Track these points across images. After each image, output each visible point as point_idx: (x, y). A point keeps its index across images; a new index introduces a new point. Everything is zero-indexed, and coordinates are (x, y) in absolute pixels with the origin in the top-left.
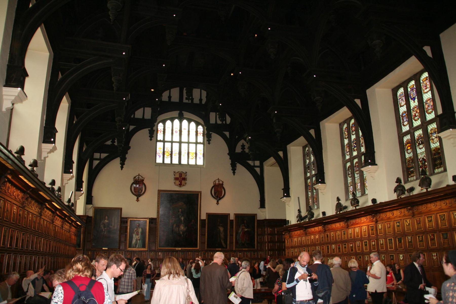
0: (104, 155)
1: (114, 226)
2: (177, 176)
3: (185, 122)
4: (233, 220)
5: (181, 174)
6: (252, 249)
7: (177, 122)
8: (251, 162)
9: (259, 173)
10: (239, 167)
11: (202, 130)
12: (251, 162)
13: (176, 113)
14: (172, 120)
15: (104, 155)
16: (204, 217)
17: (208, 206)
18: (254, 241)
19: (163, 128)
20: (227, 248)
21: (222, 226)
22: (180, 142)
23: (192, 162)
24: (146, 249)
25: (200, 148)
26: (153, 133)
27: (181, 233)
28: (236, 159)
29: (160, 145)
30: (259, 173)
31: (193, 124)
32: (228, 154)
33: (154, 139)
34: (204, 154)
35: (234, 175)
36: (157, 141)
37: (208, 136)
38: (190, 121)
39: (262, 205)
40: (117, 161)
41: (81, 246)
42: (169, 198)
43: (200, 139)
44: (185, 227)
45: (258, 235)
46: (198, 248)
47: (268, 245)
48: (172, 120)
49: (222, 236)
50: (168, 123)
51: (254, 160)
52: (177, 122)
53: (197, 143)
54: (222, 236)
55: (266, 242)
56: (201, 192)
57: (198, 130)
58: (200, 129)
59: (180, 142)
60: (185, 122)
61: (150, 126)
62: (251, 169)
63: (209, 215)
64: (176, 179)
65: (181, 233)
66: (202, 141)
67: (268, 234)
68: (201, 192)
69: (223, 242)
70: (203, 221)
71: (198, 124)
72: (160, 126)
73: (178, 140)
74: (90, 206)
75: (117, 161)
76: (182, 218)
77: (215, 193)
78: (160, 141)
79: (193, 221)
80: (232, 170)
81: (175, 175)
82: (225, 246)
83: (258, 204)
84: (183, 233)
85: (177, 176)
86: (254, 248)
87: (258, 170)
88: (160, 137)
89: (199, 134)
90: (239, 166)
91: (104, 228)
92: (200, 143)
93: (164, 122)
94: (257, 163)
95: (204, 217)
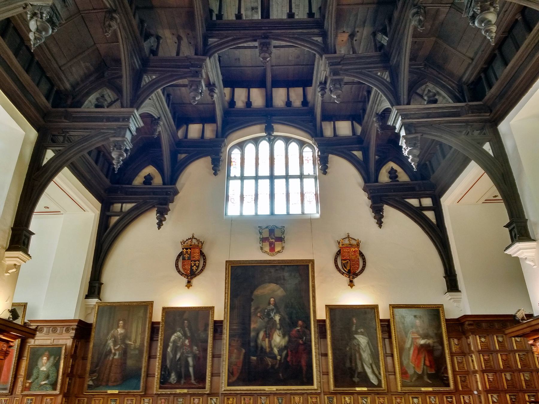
0: (127, 207)
1: (135, 342)
2: (266, 234)
3: (279, 145)
4: (324, 321)
5: (272, 231)
6: (441, 389)
7: (264, 145)
8: (414, 202)
9: (434, 220)
10: (389, 211)
11: (311, 154)
12: (414, 202)
13: (257, 131)
14: (256, 141)
15: (127, 207)
16: (321, 314)
17: (333, 293)
18: (446, 368)
19: (239, 156)
20: (380, 385)
21: (362, 334)
22: (272, 177)
23: (296, 210)
24: (57, 392)
25: (310, 185)
26: (218, 164)
27: (276, 351)
28: (381, 199)
29: (234, 186)
30: (434, 220)
31: (294, 147)
32: (364, 190)
33: (222, 174)
34: (316, 194)
35: (380, 226)
36: (229, 178)
37: (323, 163)
38: (287, 140)
39: (452, 285)
40: (152, 217)
41: (59, 386)
42: (242, 279)
43: (309, 168)
44: (284, 336)
45: (452, 354)
46: (315, 387)
47: (483, 379)
48: (256, 141)
49: (366, 355)
50: (250, 148)
51: (419, 197)
52: (264, 145)
53: (301, 177)
54: (366, 355)
55: (475, 372)
56: (312, 261)
57: (304, 154)
58: (308, 153)
59: (272, 177)
60: (279, 145)
61: (213, 152)
62: (416, 214)
63: (332, 309)
64: (263, 240)
65: (276, 351)
66: (312, 173)
67: (479, 352)
68: (312, 261)
69: (369, 371)
70: (321, 324)
71: (302, 144)
72: (236, 154)
73: (268, 174)
74: (94, 301)
75: (152, 217)
76: (277, 318)
77: (344, 266)
78: (235, 178)
79: (300, 322)
80: (375, 218)
81: (261, 233)
82: (374, 381)
83: (443, 283)
84: (281, 350)
85: (266, 234)
86: (448, 385)
87: (430, 215)
88: (235, 171)
89: (305, 162)
90: (389, 211)
91: (115, 345)
92: (309, 176)
93: (241, 146)
94: (427, 202)
95: (321, 314)
